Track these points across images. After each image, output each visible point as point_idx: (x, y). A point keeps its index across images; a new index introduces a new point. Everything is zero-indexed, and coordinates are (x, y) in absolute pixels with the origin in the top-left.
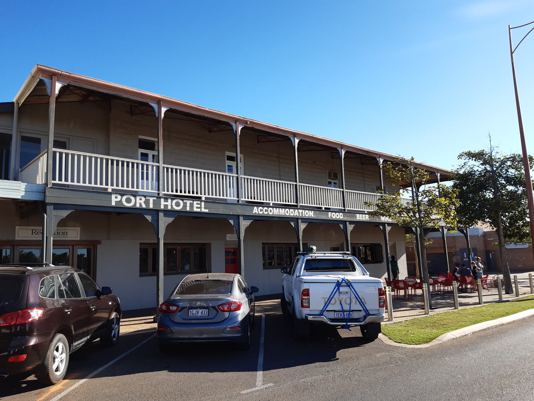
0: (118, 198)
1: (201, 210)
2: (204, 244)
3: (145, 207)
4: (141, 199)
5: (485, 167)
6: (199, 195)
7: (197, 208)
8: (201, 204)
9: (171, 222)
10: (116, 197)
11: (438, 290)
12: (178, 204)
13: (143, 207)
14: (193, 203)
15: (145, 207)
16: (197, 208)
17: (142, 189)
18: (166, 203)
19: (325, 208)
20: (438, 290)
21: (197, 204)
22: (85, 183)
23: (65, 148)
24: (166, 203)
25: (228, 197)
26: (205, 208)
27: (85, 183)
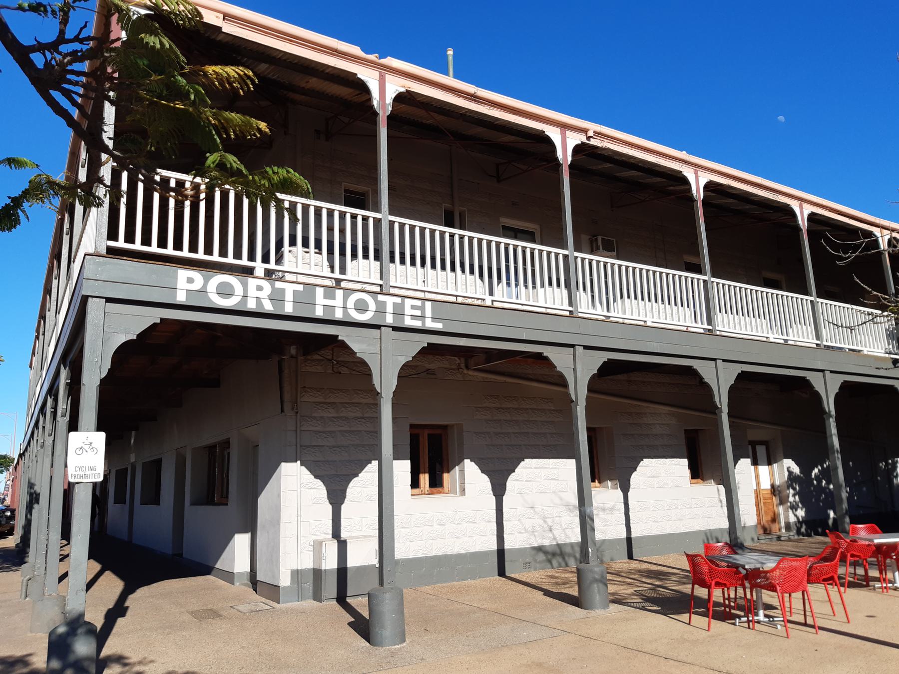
0: (264, 290)
1: (424, 323)
2: (445, 427)
3: (273, 309)
4: (259, 288)
5: (91, 82)
6: (244, 262)
7: (413, 317)
8: (422, 309)
9: (135, 338)
10: (190, 280)
11: (728, 589)
12: (225, 291)
13: (266, 308)
14: (403, 302)
15: (273, 309)
16: (413, 317)
17: (126, 241)
18: (329, 302)
19: (825, 346)
20: (728, 589)
21: (413, 307)
22: (133, 242)
23: (533, 241)
24: (329, 302)
25: (846, 344)
26: (434, 319)
27: (133, 242)
